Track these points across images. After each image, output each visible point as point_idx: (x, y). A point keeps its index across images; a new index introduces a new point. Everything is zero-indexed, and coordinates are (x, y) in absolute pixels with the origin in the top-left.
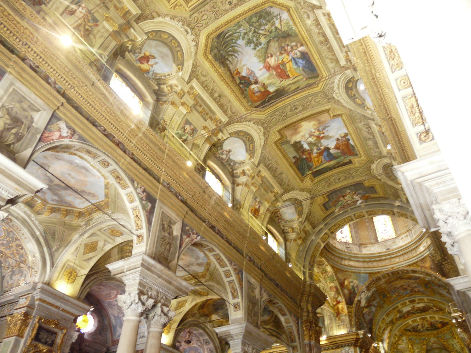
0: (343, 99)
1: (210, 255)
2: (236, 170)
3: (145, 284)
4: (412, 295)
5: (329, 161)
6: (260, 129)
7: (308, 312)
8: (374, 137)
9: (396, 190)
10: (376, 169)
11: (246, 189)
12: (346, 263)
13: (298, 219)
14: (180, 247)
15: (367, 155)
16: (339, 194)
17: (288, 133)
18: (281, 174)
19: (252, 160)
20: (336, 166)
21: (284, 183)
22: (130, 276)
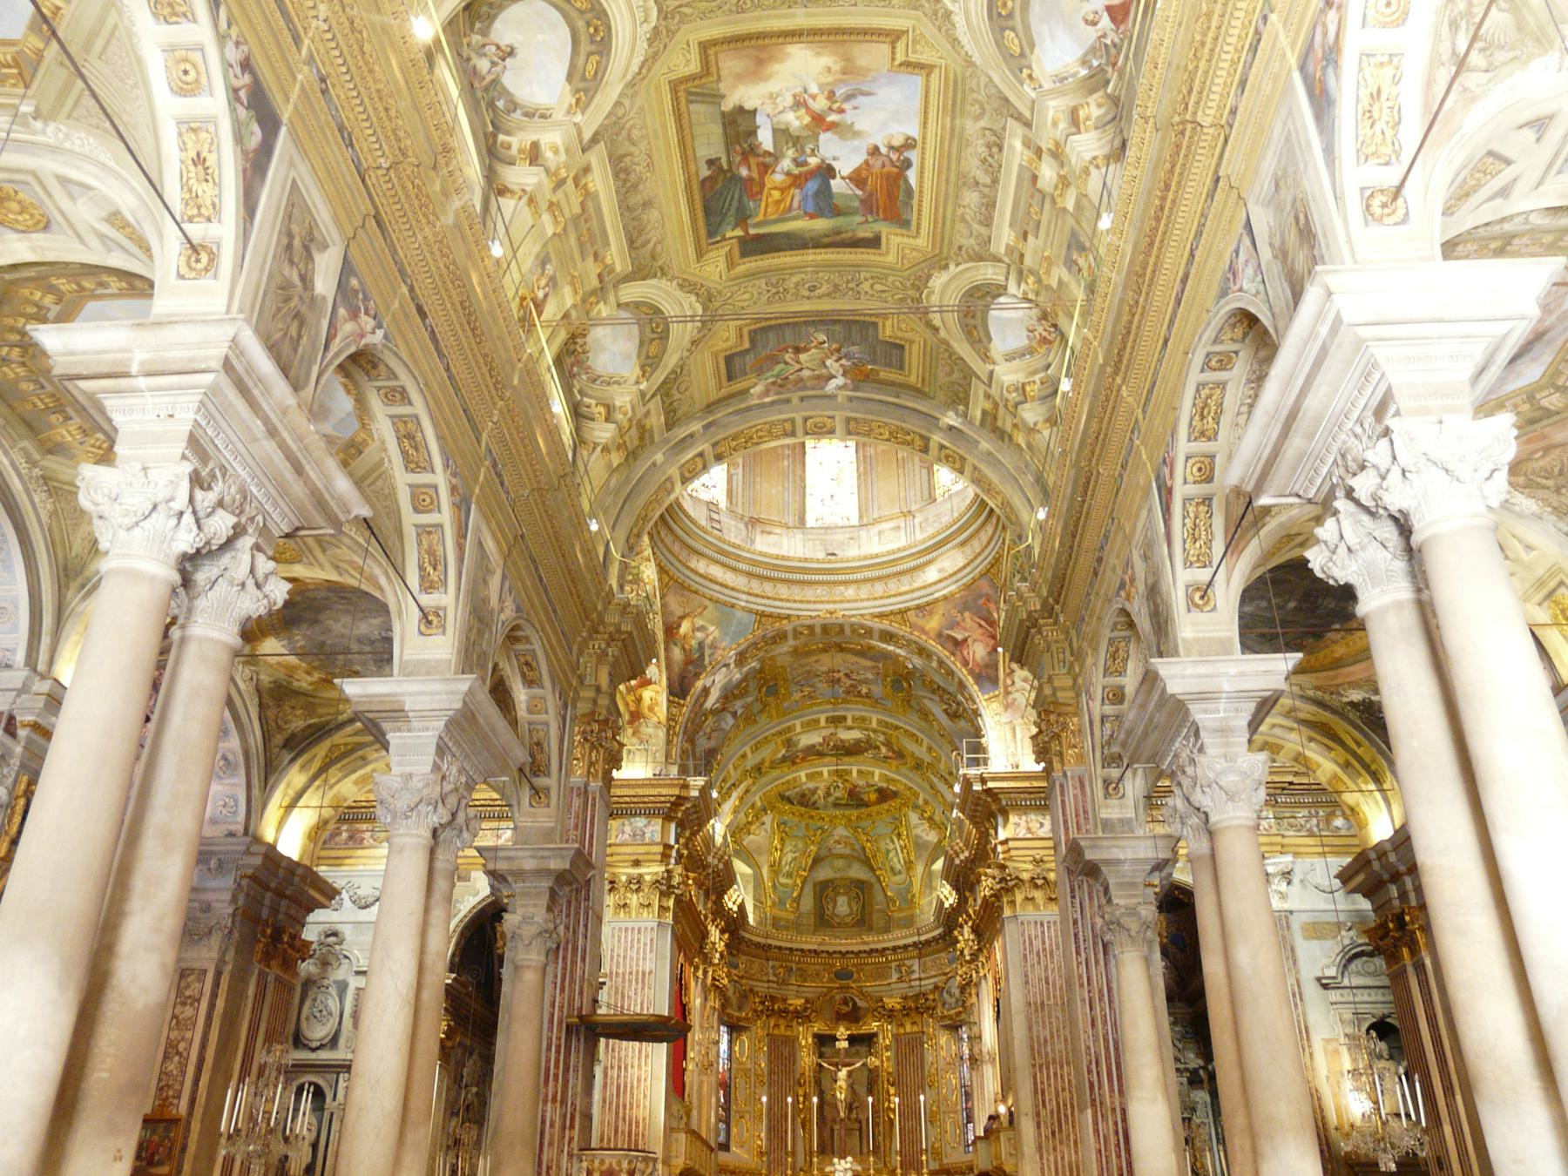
0: (967, 12)
1: (382, 416)
2: (508, 133)
3: (210, 449)
4: (845, 701)
5: (812, 217)
6: (646, 11)
7: (598, 689)
8: (995, 181)
9: (969, 374)
10: (943, 293)
11: (526, 214)
12: (701, 566)
13: (638, 383)
14: (326, 347)
15: (940, 235)
16: (789, 338)
17: (730, 64)
18: (647, 204)
19: (578, 118)
20: (826, 240)
21: (644, 238)
22: (149, 400)
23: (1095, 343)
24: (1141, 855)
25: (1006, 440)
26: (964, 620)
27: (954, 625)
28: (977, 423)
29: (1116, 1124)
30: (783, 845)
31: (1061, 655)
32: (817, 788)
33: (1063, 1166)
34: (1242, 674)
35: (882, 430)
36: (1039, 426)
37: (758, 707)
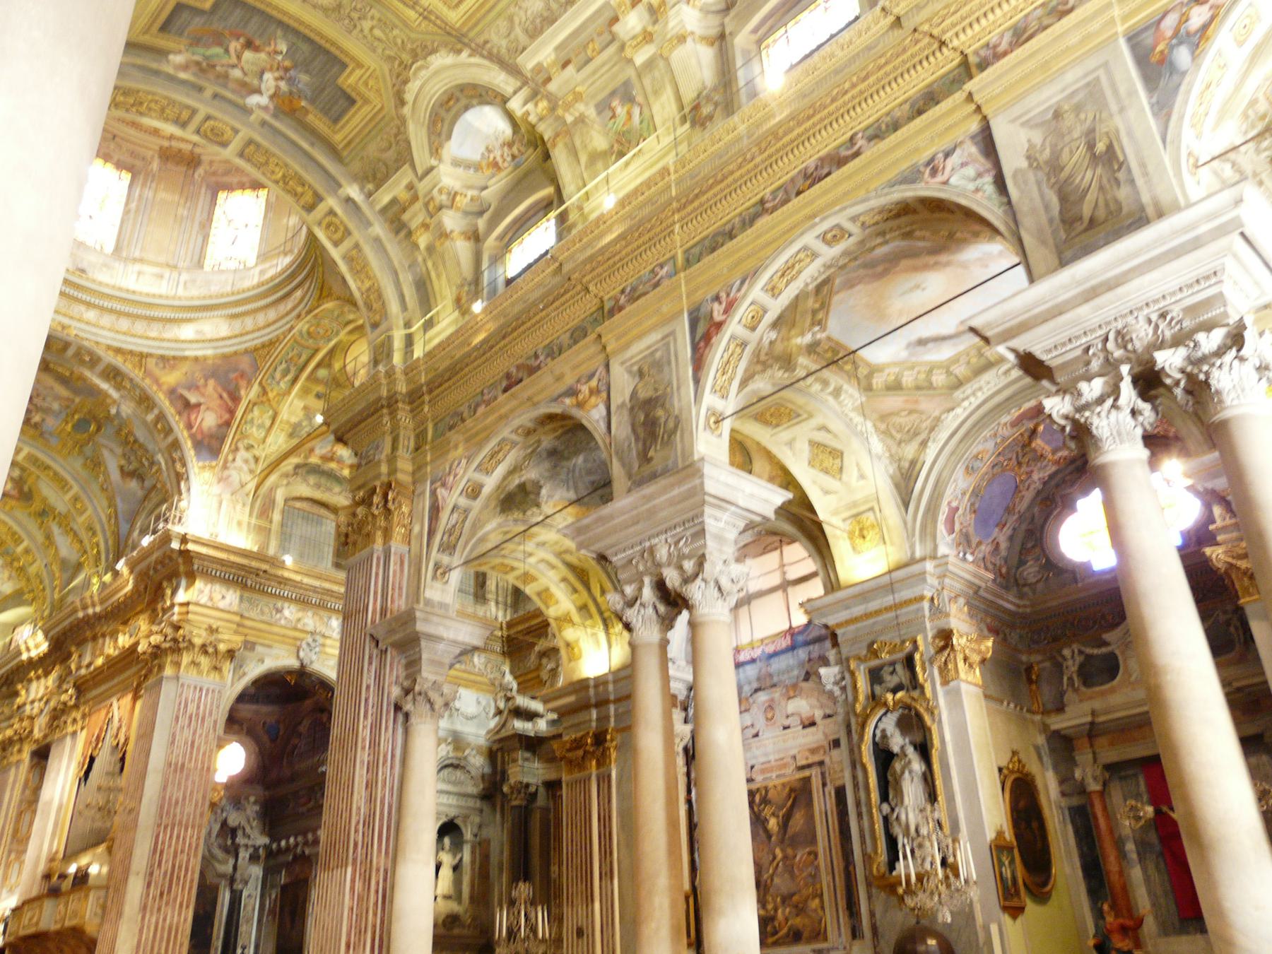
9: (405, 157)
23: (673, 177)
25: (402, 234)
26: (206, 385)
27: (193, 387)
28: (378, 207)
29: (378, 883)
33: (163, 928)
34: (752, 496)
35: (277, 169)
36: (455, 235)
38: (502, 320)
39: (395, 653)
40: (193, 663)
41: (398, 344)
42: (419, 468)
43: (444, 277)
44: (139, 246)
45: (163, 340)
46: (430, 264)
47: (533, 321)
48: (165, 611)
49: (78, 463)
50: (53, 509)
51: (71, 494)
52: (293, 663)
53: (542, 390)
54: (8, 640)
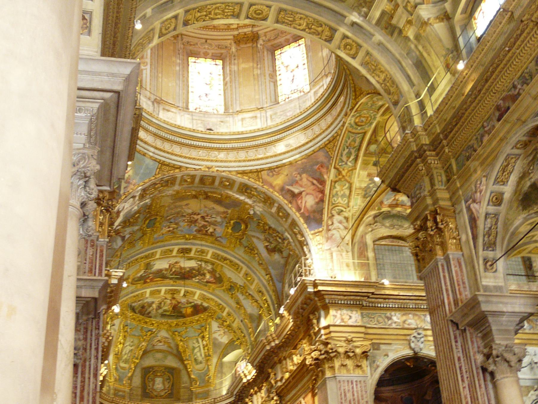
4: (195, 238)
24: (517, 309)
26: (301, 180)
27: (294, 182)
28: (374, 22)
30: (125, 340)
31: (439, 177)
32: (153, 303)
35: (302, 22)
36: (431, 21)
37: (139, 234)
38: (481, 69)
39: (472, 331)
40: (343, 365)
41: (414, 110)
42: (453, 193)
43: (433, 53)
44: (238, 102)
45: (267, 158)
46: (420, 48)
47: (504, 62)
48: (316, 334)
49: (241, 252)
50: (235, 284)
51: (243, 272)
52: (407, 352)
53: (526, 110)
54: (233, 372)
